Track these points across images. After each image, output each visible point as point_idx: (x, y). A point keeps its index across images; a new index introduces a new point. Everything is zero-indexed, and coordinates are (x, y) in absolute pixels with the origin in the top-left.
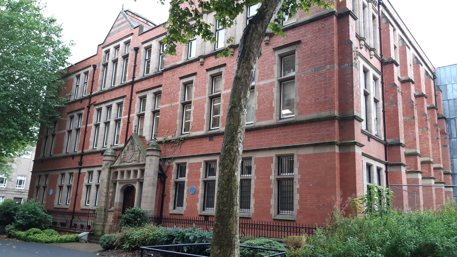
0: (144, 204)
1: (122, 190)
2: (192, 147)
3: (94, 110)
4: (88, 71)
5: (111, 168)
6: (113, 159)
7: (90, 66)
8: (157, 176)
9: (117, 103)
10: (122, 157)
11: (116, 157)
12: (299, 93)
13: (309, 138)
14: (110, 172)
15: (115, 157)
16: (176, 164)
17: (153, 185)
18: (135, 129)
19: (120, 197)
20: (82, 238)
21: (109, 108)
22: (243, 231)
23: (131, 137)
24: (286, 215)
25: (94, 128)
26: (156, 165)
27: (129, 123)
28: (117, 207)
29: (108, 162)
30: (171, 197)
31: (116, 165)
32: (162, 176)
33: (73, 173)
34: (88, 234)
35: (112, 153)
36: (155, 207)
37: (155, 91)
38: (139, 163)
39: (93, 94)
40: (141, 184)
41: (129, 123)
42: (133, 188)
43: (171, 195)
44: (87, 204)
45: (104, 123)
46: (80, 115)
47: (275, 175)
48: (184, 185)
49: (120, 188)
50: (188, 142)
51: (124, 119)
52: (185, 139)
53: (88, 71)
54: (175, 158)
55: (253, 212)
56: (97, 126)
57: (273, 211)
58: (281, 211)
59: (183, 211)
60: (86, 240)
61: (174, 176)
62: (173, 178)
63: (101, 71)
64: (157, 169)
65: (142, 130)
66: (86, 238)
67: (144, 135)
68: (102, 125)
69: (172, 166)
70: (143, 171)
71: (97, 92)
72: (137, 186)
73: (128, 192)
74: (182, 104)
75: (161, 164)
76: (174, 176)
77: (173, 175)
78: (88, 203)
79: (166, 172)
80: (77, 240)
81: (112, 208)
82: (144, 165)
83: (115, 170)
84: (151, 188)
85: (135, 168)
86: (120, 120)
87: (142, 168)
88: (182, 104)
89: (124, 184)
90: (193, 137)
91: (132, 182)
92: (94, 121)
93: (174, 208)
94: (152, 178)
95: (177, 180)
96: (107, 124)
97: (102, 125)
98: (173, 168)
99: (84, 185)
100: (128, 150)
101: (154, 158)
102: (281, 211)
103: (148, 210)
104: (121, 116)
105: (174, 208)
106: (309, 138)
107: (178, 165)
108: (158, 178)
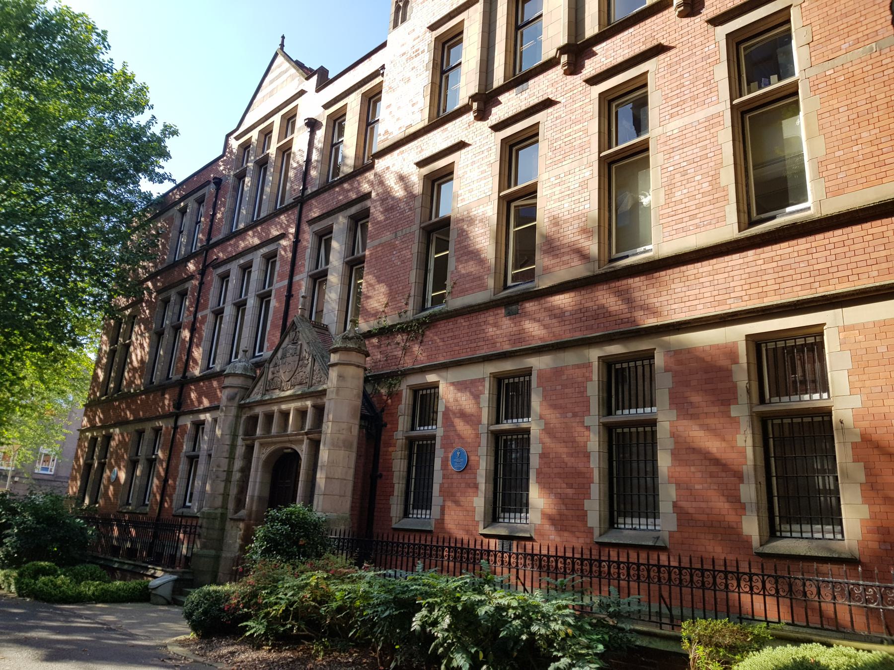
0: (321, 497)
1: (266, 462)
2: (454, 337)
3: (213, 276)
4: (204, 195)
5: (241, 407)
6: (250, 383)
7: (208, 183)
8: (357, 422)
9: (264, 256)
10: (270, 376)
11: (255, 380)
12: (822, 128)
13: (885, 266)
14: (237, 417)
15: (253, 378)
16: (411, 387)
17: (347, 445)
18: (304, 305)
19: (261, 483)
20: (159, 592)
21: (246, 269)
22: (666, 594)
23: (293, 323)
24: (634, 529)
25: (210, 318)
26: (355, 392)
27: (289, 296)
28: (254, 508)
29: (236, 390)
30: (395, 480)
31: (256, 396)
32: (373, 420)
33: (160, 428)
34: (175, 581)
35: (245, 369)
36: (352, 508)
37: (353, 210)
38: (312, 389)
39: (211, 242)
40: (315, 445)
41: (289, 296)
42: (296, 456)
43: (396, 474)
44: (188, 504)
45: (234, 304)
46: (183, 295)
47: (750, 403)
48: (433, 446)
49: (263, 457)
50: (442, 326)
51: (280, 288)
52: (434, 320)
53: (204, 195)
54: (406, 373)
55: (673, 527)
56: (218, 313)
57: (751, 527)
58: (621, 520)
59: (433, 522)
60: (170, 599)
61: (403, 423)
62: (400, 427)
63: (230, 189)
64: (359, 402)
65: (320, 312)
66: (166, 592)
67: (325, 321)
68: (229, 311)
69: (398, 395)
70: (320, 410)
71: (221, 237)
72: (303, 450)
73: (284, 471)
74: (423, 228)
75: (369, 390)
76: (403, 423)
77: (401, 420)
78: (190, 501)
79: (383, 410)
80: (144, 596)
81: (243, 513)
82: (323, 393)
83: (252, 413)
84: (342, 454)
85: (298, 404)
86: (269, 294)
87: (319, 401)
88: (423, 228)
89: (273, 448)
90: (456, 310)
91: (291, 442)
92: (212, 302)
93: (406, 514)
94: (344, 426)
95: (414, 433)
96: (240, 306)
97: (229, 311)
98: (400, 400)
99: (182, 455)
100: (284, 357)
101: (351, 371)
102: (621, 520)
103: (333, 515)
104: (271, 284)
105: (406, 514)
106: (885, 266)
107: (415, 390)
108: (361, 427)
